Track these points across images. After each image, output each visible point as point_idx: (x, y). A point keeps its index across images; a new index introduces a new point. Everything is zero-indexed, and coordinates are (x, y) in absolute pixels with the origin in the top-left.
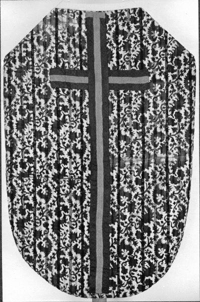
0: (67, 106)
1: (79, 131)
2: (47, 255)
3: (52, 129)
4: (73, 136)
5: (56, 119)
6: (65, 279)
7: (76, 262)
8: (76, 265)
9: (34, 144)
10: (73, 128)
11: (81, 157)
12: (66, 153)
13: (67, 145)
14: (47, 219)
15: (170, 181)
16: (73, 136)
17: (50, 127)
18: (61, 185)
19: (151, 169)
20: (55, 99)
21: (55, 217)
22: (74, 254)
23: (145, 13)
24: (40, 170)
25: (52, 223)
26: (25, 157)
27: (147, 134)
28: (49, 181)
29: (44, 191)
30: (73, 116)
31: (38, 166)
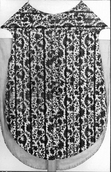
0: (75, 126)
1: (68, 112)
2: (88, 36)
3: (84, 142)
4: (72, 108)
5: (82, 148)
6: (76, 54)
7: (70, 33)
8: (70, 32)
9: (95, 102)
10: (72, 113)
11: (67, 96)
12: (76, 98)
13: (75, 103)
14: (87, 57)
15: (14, 82)
16: (72, 48)
17: (85, 112)
18: (79, 47)
19: (25, 59)
20: (83, 129)
21: (82, 118)
22: (71, 38)
23: (28, 152)
24: (91, 87)
25: (84, 55)
26: (100, 94)
27: (28, 111)
28: (86, 48)
29: (89, 42)
30: (72, 120)
31: (93, 89)
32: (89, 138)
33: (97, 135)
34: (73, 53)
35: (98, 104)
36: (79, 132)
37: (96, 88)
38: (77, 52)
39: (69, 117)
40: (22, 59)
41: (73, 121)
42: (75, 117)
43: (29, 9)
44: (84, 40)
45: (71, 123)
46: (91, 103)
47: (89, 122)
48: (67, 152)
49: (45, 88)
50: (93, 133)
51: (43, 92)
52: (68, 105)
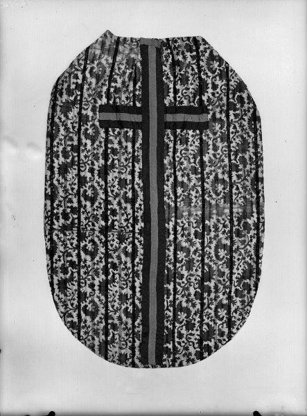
9: (78, 307)
15: (234, 235)
16: (122, 183)
22: (123, 258)
26: (68, 207)
30: (123, 160)
31: (83, 217)
32: (91, 123)
33: (75, 191)
35: (73, 189)
36: (110, 196)
37: (76, 221)
38: (114, 289)
39: (129, 167)
42: (117, 340)
44: (99, 312)
45: (126, 155)
46: (85, 191)
47: (89, 153)
48: (133, 336)
49: (175, 289)
50: (82, 132)
51: (179, 221)
52: (129, 190)
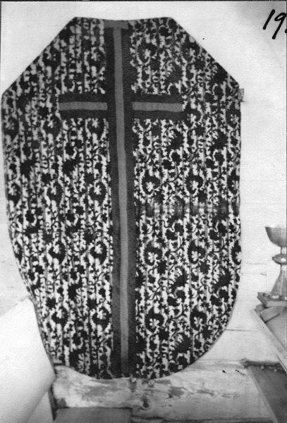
34: (90, 293)
40: (192, 220)
41: (85, 149)
43: (158, 286)
